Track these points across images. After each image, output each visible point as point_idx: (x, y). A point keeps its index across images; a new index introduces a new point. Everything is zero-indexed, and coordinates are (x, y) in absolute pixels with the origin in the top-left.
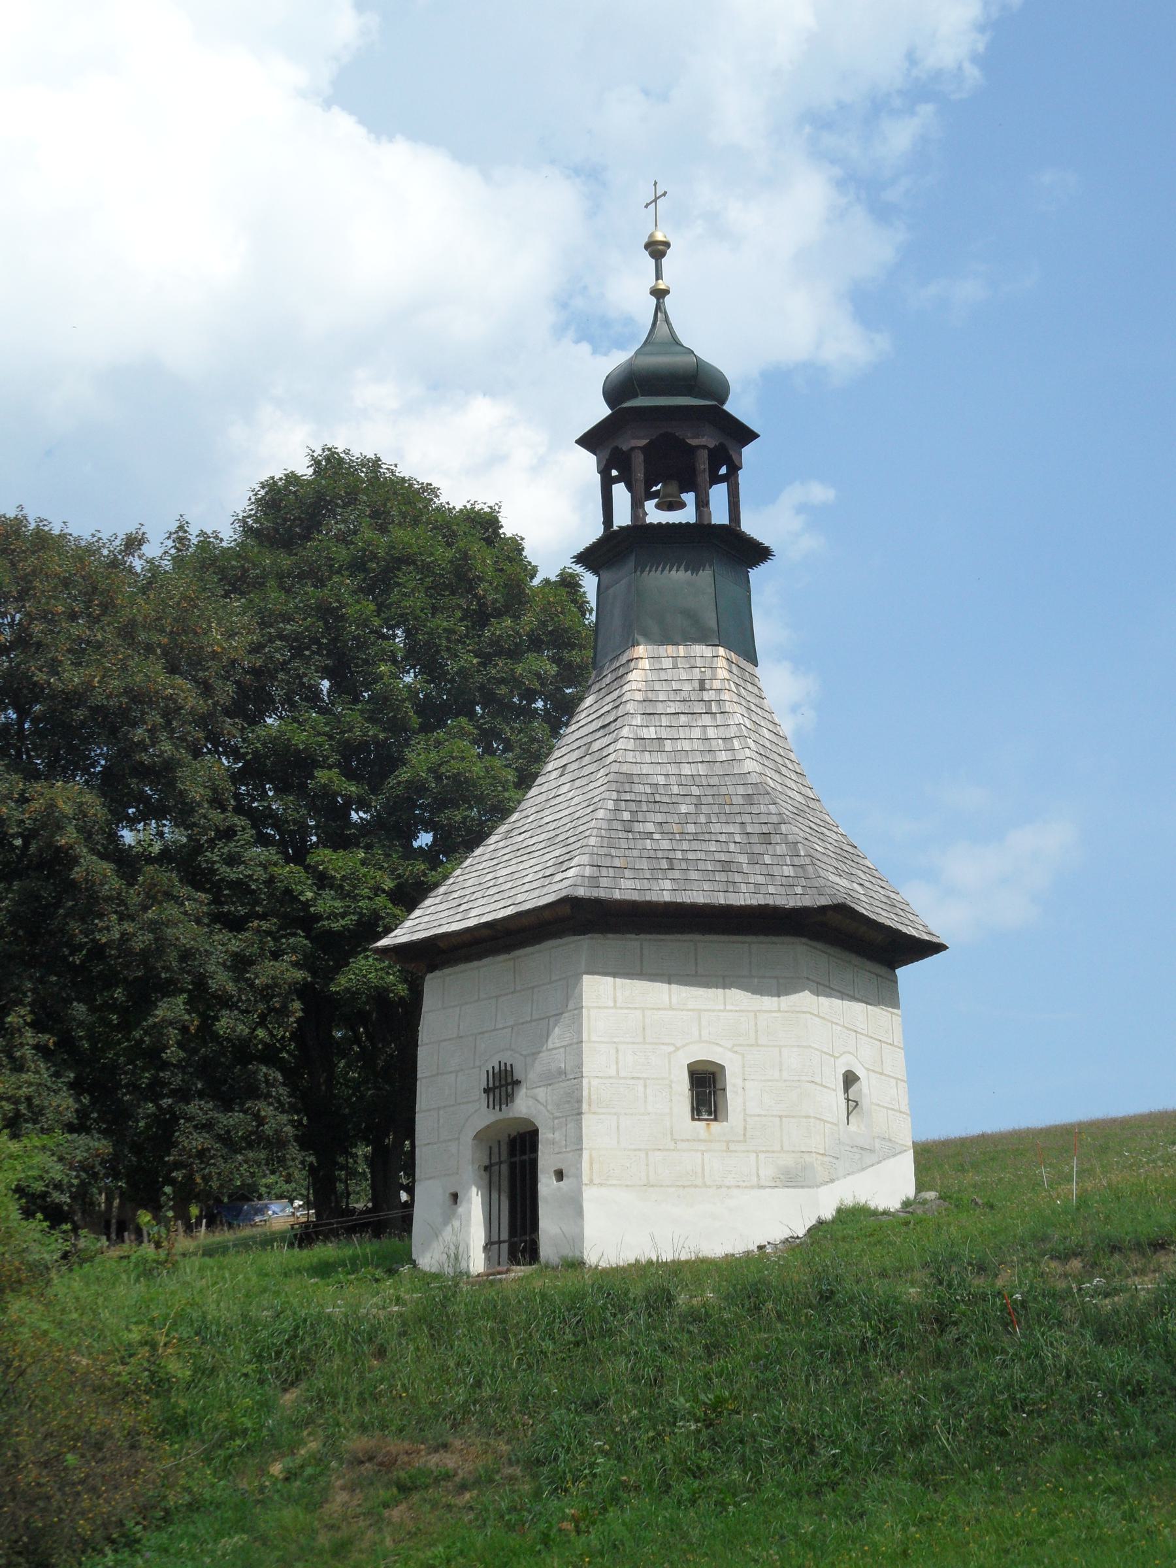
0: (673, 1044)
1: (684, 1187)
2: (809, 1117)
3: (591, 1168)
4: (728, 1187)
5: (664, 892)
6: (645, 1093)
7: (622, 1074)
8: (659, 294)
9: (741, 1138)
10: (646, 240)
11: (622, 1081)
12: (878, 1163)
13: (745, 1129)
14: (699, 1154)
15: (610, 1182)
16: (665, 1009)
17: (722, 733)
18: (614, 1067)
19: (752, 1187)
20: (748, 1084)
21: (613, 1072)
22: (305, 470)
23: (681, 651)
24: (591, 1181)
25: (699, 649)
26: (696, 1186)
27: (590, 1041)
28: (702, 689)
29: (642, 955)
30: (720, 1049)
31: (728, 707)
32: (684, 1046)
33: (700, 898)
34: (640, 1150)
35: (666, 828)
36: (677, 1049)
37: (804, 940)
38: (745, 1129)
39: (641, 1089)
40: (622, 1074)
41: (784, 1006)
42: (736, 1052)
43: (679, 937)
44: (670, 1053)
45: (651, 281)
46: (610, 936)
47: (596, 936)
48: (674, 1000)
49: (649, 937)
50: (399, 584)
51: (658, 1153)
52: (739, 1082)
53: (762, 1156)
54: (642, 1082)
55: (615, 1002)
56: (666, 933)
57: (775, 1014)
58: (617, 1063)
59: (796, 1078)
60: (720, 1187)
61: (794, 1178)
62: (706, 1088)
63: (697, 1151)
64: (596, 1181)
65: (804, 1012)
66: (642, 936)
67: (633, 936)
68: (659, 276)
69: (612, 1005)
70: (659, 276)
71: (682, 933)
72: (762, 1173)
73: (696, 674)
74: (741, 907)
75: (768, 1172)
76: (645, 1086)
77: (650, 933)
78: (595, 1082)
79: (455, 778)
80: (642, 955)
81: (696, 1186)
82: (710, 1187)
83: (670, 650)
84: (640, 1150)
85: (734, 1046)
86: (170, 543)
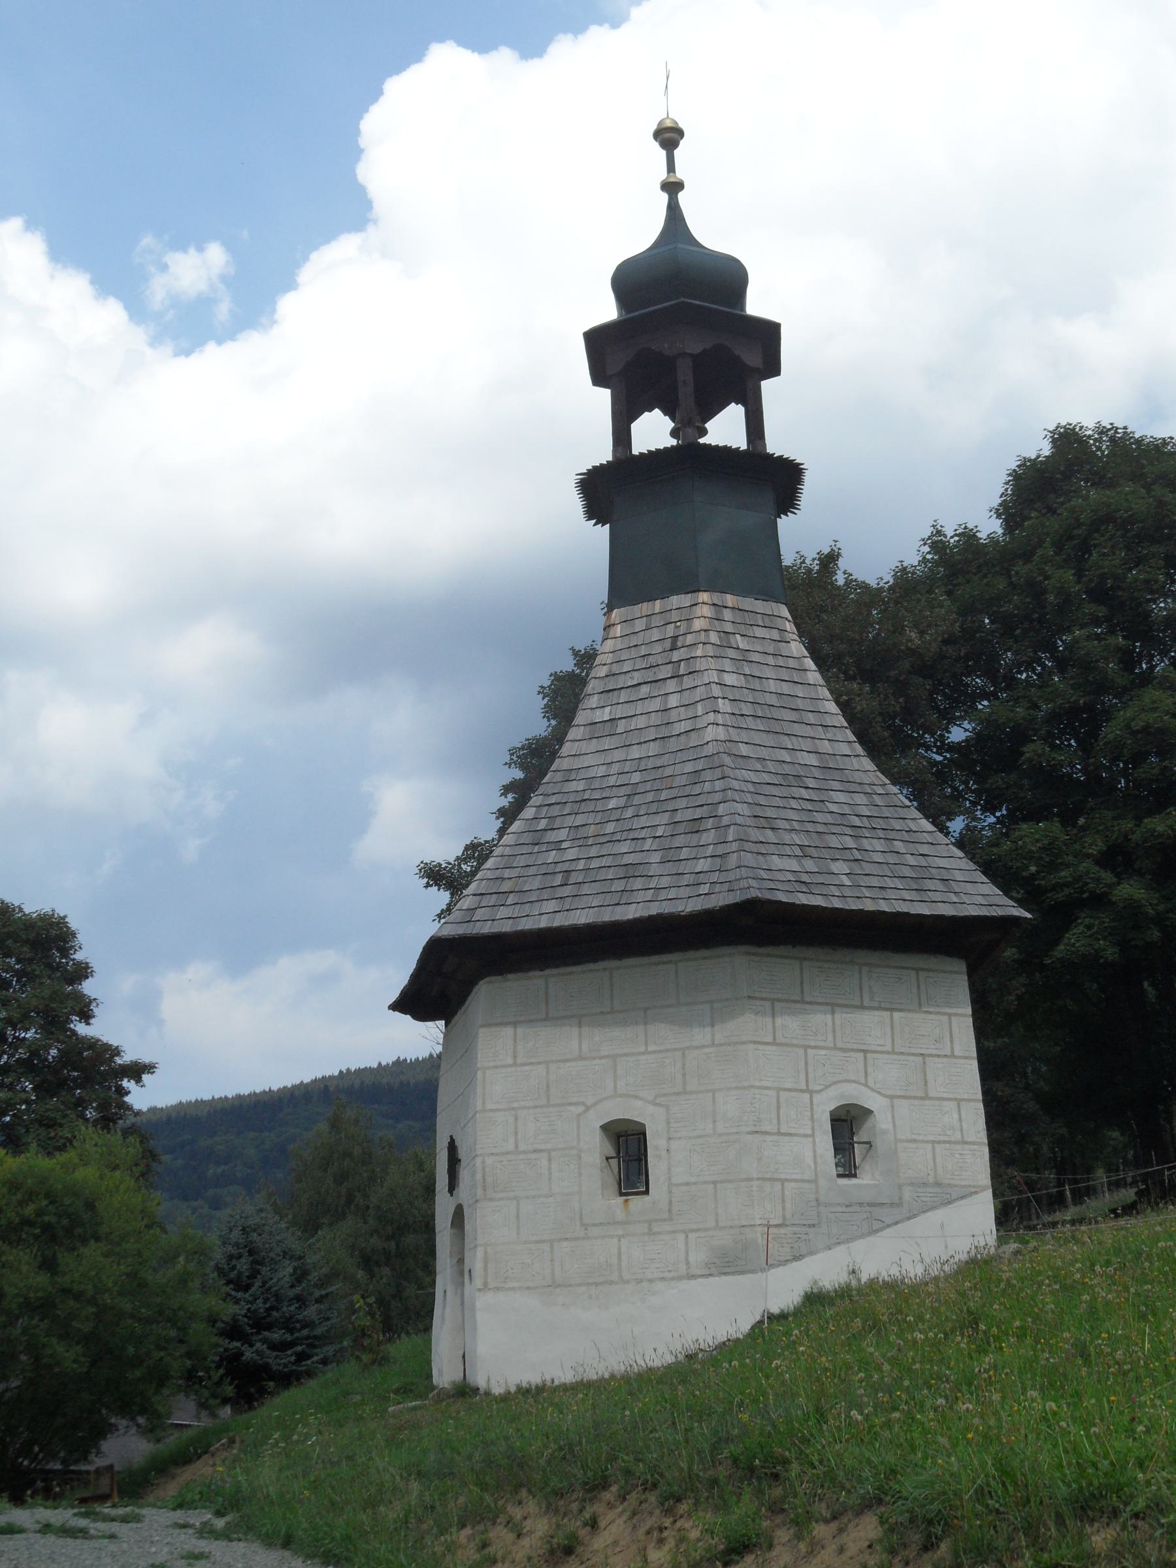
0: (583, 1104)
1: (596, 1284)
2: (751, 1180)
3: (485, 1269)
4: (651, 1281)
5: (544, 916)
6: (550, 1169)
7: (522, 1147)
8: (672, 188)
9: (666, 1215)
10: (655, 127)
11: (522, 1157)
12: (909, 1218)
13: (670, 1203)
14: (615, 1240)
15: (507, 1286)
16: (574, 1060)
17: (687, 698)
18: (512, 1140)
19: (680, 1278)
20: (674, 1145)
21: (511, 1146)
22: (1046, 449)
23: (658, 605)
24: (485, 1284)
25: (675, 601)
26: (612, 1283)
27: (484, 1111)
28: (674, 648)
29: (612, 985)
30: (639, 1103)
31: (700, 665)
32: (595, 1104)
33: (582, 918)
34: (543, 1241)
35: (582, 832)
36: (588, 1109)
37: (743, 948)
38: (670, 1203)
39: (545, 1163)
40: (522, 1147)
41: (719, 1038)
42: (659, 1105)
43: (591, 966)
44: (579, 1115)
45: (663, 174)
46: (510, 976)
47: (493, 978)
48: (585, 1047)
49: (555, 971)
50: (1095, 546)
51: (565, 1244)
52: (662, 1143)
53: (692, 1236)
54: (545, 1154)
55: (515, 1057)
56: (574, 964)
57: (707, 1050)
58: (516, 1133)
59: (735, 1130)
60: (641, 1281)
61: (728, 1263)
62: (629, 1149)
63: (611, 1237)
64: (492, 1285)
65: (743, 1043)
66: (548, 972)
67: (538, 973)
68: (671, 167)
69: (510, 1061)
70: (671, 167)
71: (595, 961)
72: (692, 1258)
73: (670, 631)
74: (629, 921)
75: (698, 1257)
76: (550, 1160)
77: (557, 966)
78: (489, 1161)
79: (1145, 730)
80: (612, 985)
81: (612, 1283)
82: (628, 1282)
83: (645, 608)
84: (543, 1241)
85: (656, 1098)
86: (927, 549)
